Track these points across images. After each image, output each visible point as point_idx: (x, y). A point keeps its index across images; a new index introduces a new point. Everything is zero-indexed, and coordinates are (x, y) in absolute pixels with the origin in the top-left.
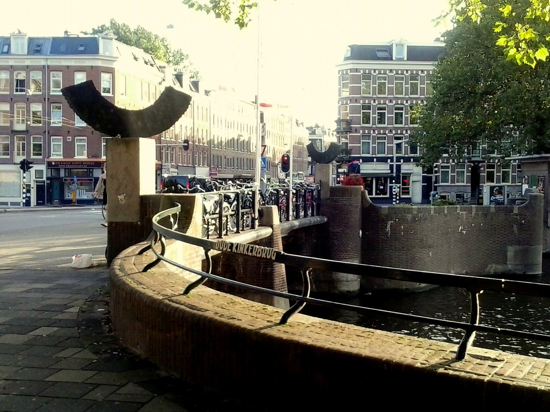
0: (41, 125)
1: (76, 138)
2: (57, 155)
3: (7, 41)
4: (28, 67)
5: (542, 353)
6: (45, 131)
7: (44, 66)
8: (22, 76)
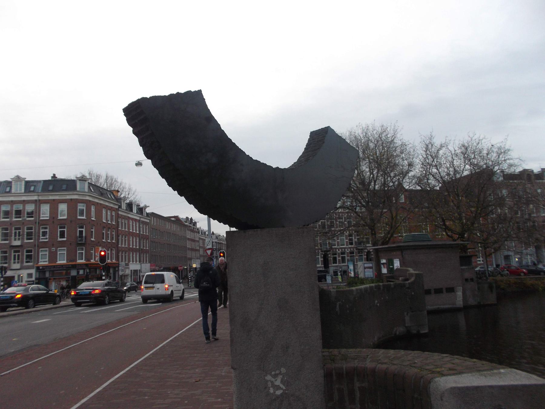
0: (32, 241)
1: (59, 249)
2: (44, 261)
3: (8, 184)
4: (24, 201)
5: (210, 313)
6: (35, 245)
7: (36, 200)
8: (20, 207)
